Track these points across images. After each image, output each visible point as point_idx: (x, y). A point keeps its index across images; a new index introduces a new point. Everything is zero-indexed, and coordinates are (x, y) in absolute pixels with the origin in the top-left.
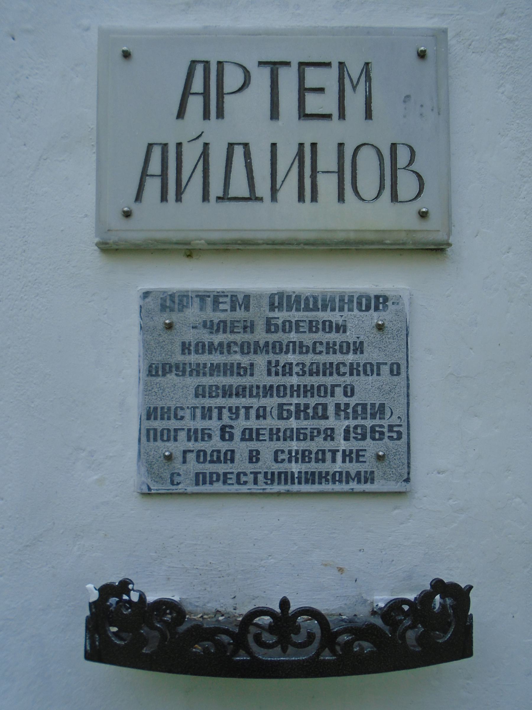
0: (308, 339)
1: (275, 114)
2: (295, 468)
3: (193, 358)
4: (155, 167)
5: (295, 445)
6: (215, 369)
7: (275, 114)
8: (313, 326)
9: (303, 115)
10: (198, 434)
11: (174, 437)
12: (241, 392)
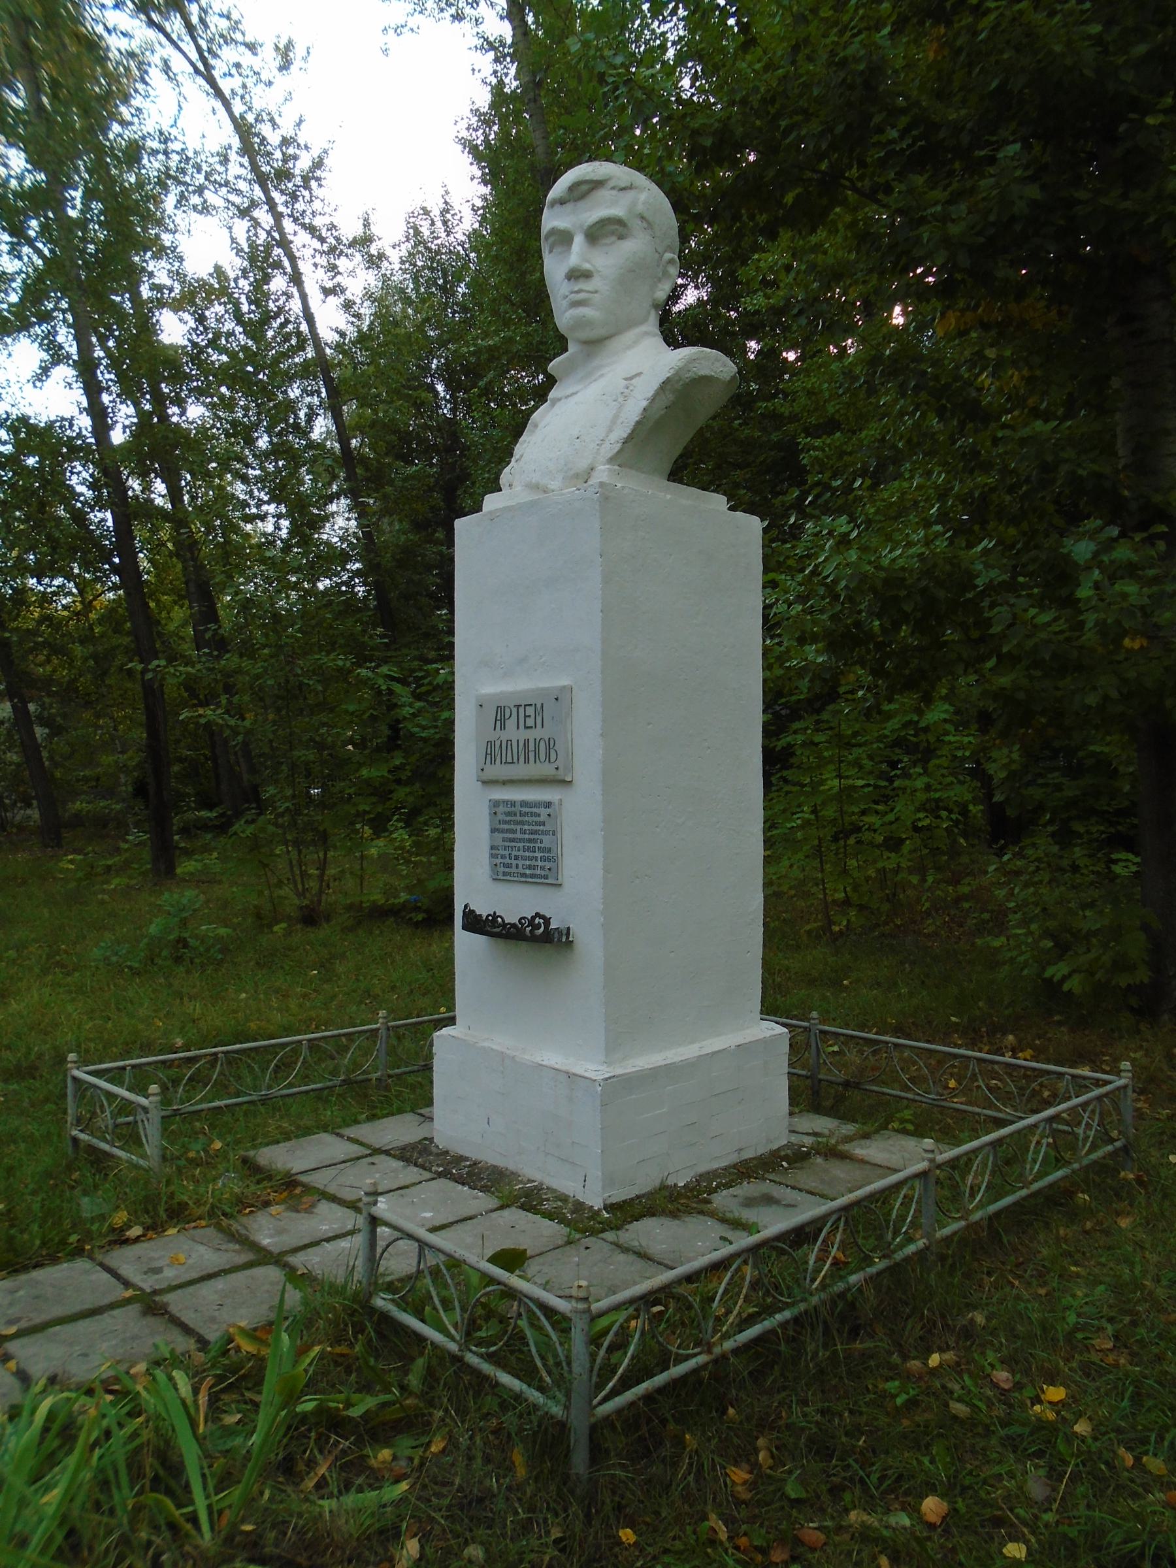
0: (531, 819)
2: (528, 872)
5: (528, 863)
9: (526, 727)
10: (220, 1108)
11: (604, 223)
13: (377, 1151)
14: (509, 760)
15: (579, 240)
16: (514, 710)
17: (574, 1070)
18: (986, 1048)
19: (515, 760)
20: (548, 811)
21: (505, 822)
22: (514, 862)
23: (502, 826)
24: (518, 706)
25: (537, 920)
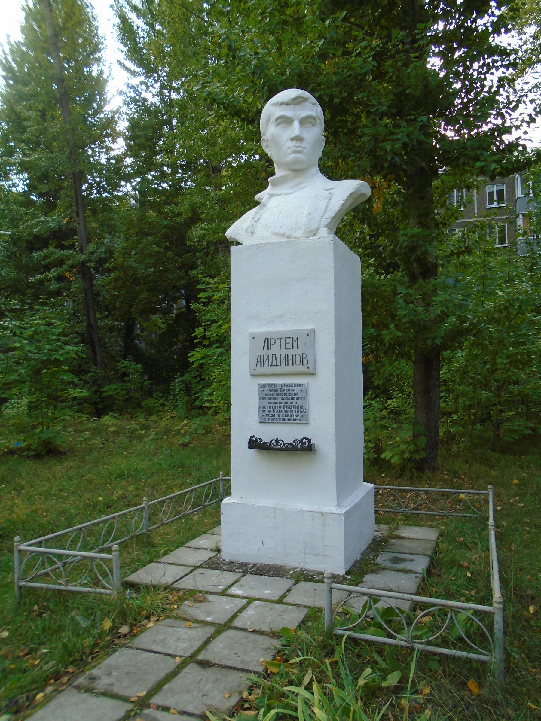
0: (288, 393)
2: (286, 418)
9: (286, 348)
13: (195, 568)
14: (274, 363)
15: (296, 124)
16: (278, 341)
17: (324, 510)
18: (449, 486)
19: (279, 364)
20: (300, 388)
21: (269, 395)
22: (276, 414)
23: (267, 397)
24: (280, 339)
25: (304, 441)
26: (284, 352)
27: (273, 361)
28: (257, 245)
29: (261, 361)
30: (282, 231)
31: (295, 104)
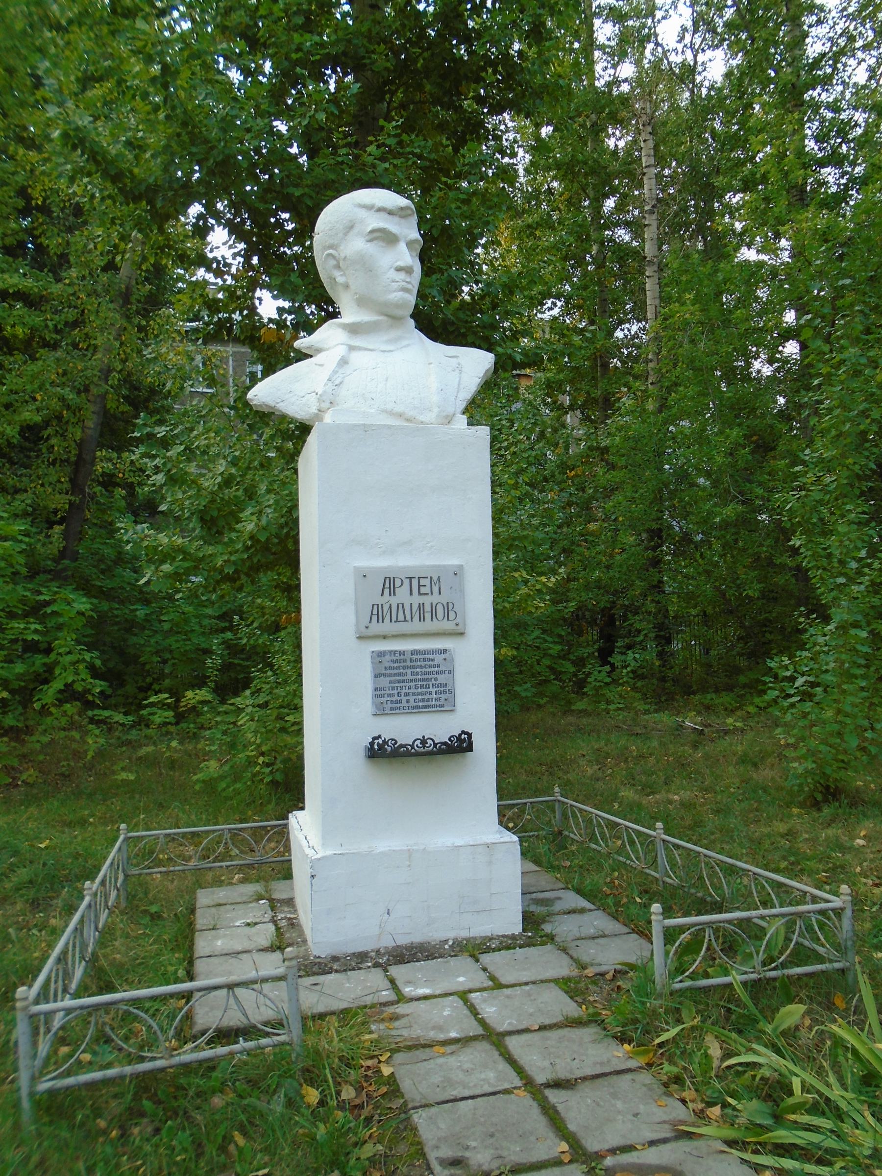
0: (423, 664)
1: (411, 594)
2: (420, 704)
3: (388, 672)
4: (375, 612)
6: (395, 675)
7: (411, 594)
8: (424, 660)
9: (420, 594)
12: (403, 681)
26: (416, 600)
27: (399, 614)
28: (364, 425)
29: (378, 613)
30: (399, 409)
31: (401, 217)
